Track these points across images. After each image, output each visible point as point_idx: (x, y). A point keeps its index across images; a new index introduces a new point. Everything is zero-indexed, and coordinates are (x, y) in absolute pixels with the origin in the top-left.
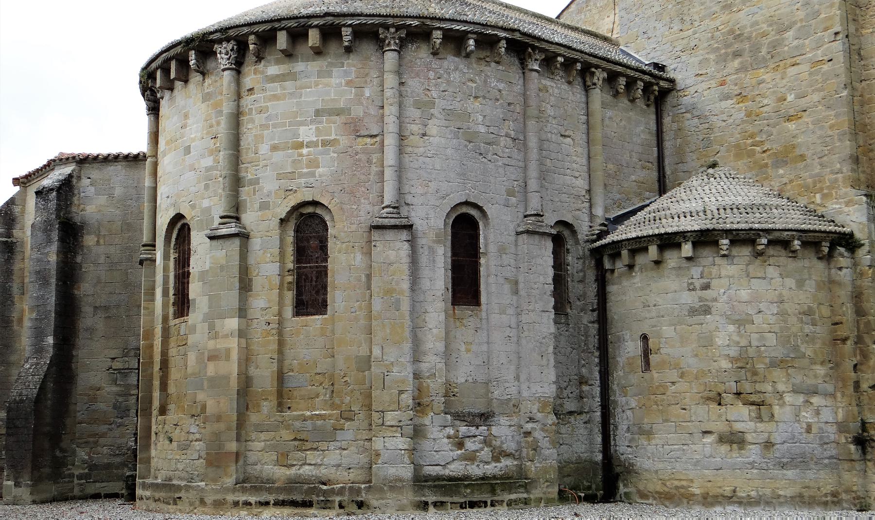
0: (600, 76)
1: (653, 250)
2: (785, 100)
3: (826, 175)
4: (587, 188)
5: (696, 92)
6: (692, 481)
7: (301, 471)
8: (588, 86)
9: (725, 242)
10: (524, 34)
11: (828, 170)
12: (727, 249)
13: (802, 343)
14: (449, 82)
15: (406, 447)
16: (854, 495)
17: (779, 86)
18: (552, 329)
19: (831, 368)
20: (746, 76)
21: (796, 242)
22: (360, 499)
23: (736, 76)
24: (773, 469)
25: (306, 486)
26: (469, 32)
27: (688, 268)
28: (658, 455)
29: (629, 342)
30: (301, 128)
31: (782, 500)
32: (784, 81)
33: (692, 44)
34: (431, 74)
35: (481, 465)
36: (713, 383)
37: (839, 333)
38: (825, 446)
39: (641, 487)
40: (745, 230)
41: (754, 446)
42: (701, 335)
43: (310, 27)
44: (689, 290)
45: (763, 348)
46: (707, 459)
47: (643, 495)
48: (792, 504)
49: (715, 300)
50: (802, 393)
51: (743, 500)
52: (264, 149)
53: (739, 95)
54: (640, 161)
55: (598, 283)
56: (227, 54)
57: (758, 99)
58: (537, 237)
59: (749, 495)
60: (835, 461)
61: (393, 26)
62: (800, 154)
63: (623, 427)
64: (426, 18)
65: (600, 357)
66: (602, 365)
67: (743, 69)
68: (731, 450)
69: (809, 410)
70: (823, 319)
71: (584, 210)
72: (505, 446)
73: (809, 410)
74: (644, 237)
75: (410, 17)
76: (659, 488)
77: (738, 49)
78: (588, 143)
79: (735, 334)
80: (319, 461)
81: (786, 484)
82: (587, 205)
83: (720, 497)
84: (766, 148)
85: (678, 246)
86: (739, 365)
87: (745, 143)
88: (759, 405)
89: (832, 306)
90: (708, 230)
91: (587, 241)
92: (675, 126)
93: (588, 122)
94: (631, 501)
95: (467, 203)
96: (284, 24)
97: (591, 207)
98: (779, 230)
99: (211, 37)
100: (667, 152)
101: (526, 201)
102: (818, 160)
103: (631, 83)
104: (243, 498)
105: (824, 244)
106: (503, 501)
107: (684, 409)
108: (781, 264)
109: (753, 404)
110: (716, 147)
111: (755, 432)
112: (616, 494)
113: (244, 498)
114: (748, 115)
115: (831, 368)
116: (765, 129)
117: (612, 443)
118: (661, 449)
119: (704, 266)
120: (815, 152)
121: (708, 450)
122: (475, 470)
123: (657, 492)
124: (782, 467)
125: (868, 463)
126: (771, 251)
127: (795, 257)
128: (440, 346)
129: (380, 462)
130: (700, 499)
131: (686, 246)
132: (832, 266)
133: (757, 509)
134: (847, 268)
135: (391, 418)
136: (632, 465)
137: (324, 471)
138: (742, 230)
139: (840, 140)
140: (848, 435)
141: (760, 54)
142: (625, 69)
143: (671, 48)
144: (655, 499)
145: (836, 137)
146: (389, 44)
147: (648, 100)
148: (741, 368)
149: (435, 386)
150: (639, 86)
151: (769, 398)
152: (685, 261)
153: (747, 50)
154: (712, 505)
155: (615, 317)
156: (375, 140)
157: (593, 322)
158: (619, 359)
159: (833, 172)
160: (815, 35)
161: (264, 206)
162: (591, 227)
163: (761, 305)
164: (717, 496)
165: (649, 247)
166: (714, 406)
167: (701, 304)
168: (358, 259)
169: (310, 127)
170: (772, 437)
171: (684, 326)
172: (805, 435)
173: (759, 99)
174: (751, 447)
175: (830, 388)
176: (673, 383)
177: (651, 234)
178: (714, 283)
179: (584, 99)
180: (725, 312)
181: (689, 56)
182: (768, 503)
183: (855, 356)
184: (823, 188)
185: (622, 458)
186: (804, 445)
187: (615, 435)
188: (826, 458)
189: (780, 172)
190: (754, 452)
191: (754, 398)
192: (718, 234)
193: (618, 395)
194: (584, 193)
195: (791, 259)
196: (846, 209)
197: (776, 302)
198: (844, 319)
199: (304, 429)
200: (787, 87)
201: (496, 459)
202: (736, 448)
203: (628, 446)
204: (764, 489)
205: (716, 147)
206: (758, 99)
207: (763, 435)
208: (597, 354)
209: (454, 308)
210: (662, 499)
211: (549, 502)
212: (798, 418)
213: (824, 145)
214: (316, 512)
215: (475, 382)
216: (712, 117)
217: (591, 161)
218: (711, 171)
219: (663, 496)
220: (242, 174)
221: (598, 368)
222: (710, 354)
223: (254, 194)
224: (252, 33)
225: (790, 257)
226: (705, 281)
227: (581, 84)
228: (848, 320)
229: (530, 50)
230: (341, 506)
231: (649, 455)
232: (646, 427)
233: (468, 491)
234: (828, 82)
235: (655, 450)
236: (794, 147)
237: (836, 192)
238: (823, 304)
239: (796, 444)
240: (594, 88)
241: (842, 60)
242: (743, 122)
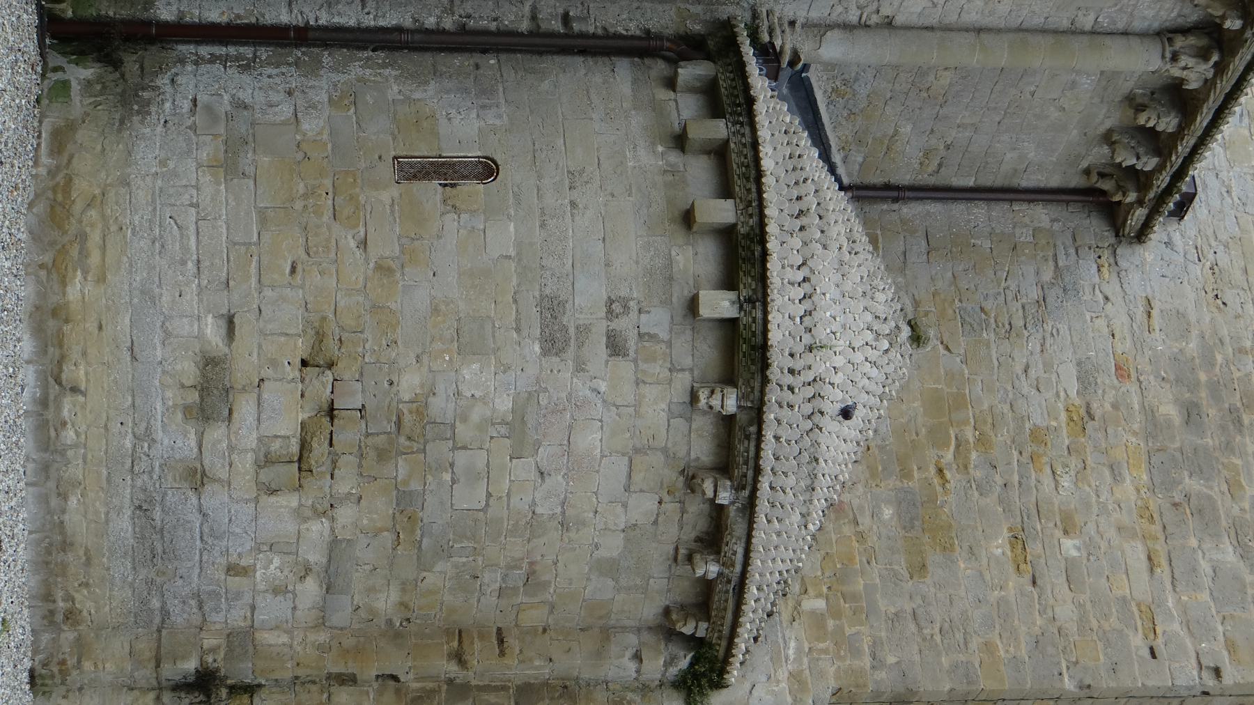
1: (723, 212)
2: (1066, 532)
3: (872, 627)
4: (900, 20)
5: (1107, 298)
6: (101, 279)
8: (1170, 40)
9: (731, 405)
11: (883, 634)
12: (711, 407)
13: (456, 566)
16: (71, 662)
17: (1102, 520)
19: (390, 622)
20: (1135, 434)
21: (713, 569)
23: (1136, 407)
24: (133, 487)
27: (666, 302)
28: (171, 191)
29: (477, 124)
32: (1112, 533)
33: (1229, 295)
36: (360, 349)
37: (477, 645)
38: (193, 602)
39: (82, 135)
40: (757, 456)
41: (193, 444)
42: (488, 327)
44: (610, 302)
45: (447, 477)
46: (159, 324)
47: (61, 140)
48: (44, 525)
49: (580, 368)
50: (329, 561)
51: (52, 409)
53: (1088, 413)
54: (948, 147)
55: (639, 38)
57: (1074, 462)
59: (64, 424)
60: (157, 620)
62: (928, 563)
63: (245, 86)
66: (417, 37)
67: (1153, 426)
68: (183, 386)
69: (286, 573)
70: (514, 612)
71: (839, 9)
73: (286, 573)
74: (760, 192)
76: (82, 187)
77: (1204, 416)
78: (1020, 30)
79: (489, 413)
81: (97, 512)
82: (853, 17)
83: (57, 352)
84: (948, 475)
85: (729, 282)
86: (407, 419)
87: (966, 422)
88: (300, 460)
89: (545, 630)
90: (765, 365)
91: (755, 15)
92: (1024, 236)
93: (1074, 32)
94: (45, 102)
97: (847, 27)
98: (749, 537)
100: (958, 210)
102: (908, 607)
103: (1158, 143)
105: (703, 625)
107: (293, 270)
108: (661, 528)
109: (304, 445)
110: (962, 344)
111: (231, 448)
112: (64, 54)
114: (1038, 436)
115: (390, 622)
116: (998, 478)
117: (204, 51)
118: (185, 199)
119: (669, 344)
120: (929, 604)
121: (184, 327)
123: (69, 180)
124: (140, 507)
125: (152, 695)
126: (696, 508)
127: (675, 560)
130: (54, 299)
131: (727, 304)
132: (647, 637)
133: (27, 443)
134: (638, 671)
136: (144, 112)
138: (758, 449)
139: (955, 667)
140: (222, 655)
141: (1186, 473)
142: (1199, 133)
143: (1223, 237)
144: (52, 173)
145: (962, 658)
147: (1102, 175)
148: (399, 423)
150: (1144, 159)
151: (318, 487)
152: (686, 293)
153: (1199, 442)
154: (38, 330)
155: (546, 85)
157: (534, 18)
158: (432, 86)
159: (876, 644)
160: (1218, 619)
162: (792, 23)
163: (560, 478)
164: (61, 346)
165: (730, 202)
166: (301, 348)
167: (572, 331)
170: (216, 486)
171: (514, 282)
172: (222, 561)
173: (1073, 466)
174: (192, 436)
175: (341, 616)
176: (364, 244)
177: (767, 212)
178: (625, 368)
179: (1138, 25)
180: (546, 390)
181: (1200, 286)
182: (45, 469)
183: (418, 679)
184: (840, 619)
185: (163, 81)
186: (197, 558)
187: (224, 60)
188: (164, 603)
189: (887, 512)
190: (179, 443)
191: (319, 448)
192: (753, 388)
193: (335, 77)
194: (886, 11)
195: (672, 552)
196: (783, 674)
197: (563, 513)
198: (511, 661)
200: (1098, 539)
202: (189, 400)
203: (195, 101)
204: (80, 461)
205: (962, 344)
206: (1074, 462)
207: (223, 466)
208: (448, 24)
210: (50, 194)
212: (265, 548)
213: (946, 625)
216: (1039, 336)
217: (971, 37)
218: (906, 332)
219: (60, 197)
221: (408, 23)
222: (438, 345)
225: (677, 549)
226: (632, 344)
227: (1180, 20)
228: (509, 668)
231: (171, 165)
232: (247, 160)
234: (1100, 646)
235: (184, 182)
236: (947, 549)
237: (825, 651)
238: (551, 612)
239: (198, 542)
240: (1163, 57)
241: (1150, 683)
242: (1021, 420)
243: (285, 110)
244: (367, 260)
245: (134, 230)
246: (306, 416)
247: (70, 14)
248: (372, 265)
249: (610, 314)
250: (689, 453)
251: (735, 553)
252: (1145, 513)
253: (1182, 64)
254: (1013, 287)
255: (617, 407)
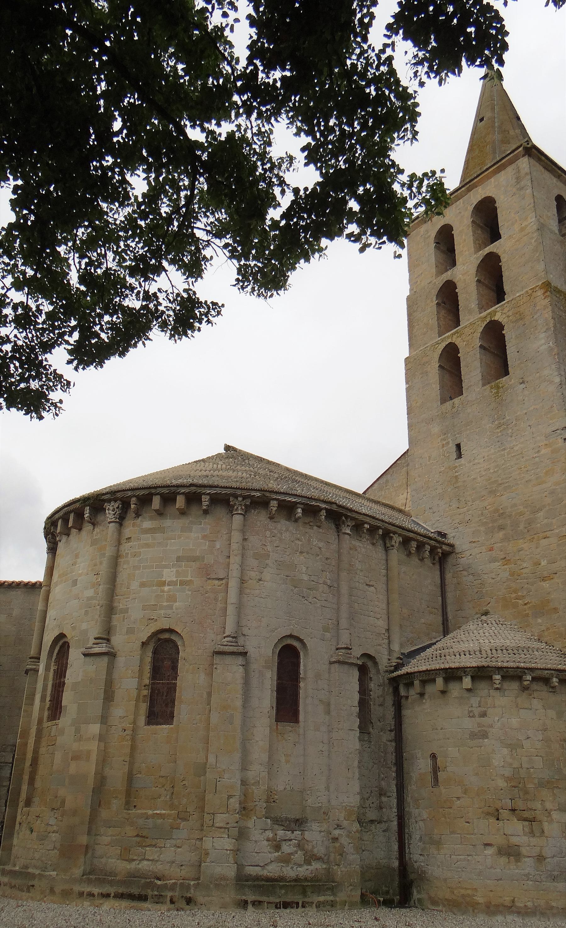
0: (397, 540)
1: (440, 681)
2: (540, 564)
6: (476, 889)
7: (140, 866)
9: (498, 677)
10: (340, 506)
14: (280, 539)
15: (231, 847)
18: (357, 745)
20: (509, 545)
22: (189, 895)
25: (143, 881)
26: (298, 503)
30: (165, 570)
31: (555, 911)
34: (268, 533)
35: (295, 868)
40: (513, 668)
43: (179, 493)
45: (532, 770)
47: (435, 902)
49: (491, 726)
52: (135, 585)
54: (428, 607)
56: (113, 510)
57: (519, 562)
58: (346, 667)
59: (525, 905)
61: (241, 495)
63: (416, 836)
64: (266, 491)
65: (397, 772)
66: (399, 779)
68: (509, 862)
71: (384, 646)
72: (315, 851)
74: (432, 670)
75: (254, 490)
80: (156, 857)
82: (386, 641)
85: (460, 679)
86: (513, 784)
88: (531, 822)
91: (387, 671)
93: (387, 575)
95: (291, 636)
96: (159, 490)
97: (389, 643)
98: (540, 669)
99: (103, 497)
101: (338, 637)
103: (420, 546)
104: (87, 889)
106: (312, 903)
109: (525, 820)
111: (529, 846)
112: (411, 900)
113: (88, 890)
114: (512, 574)
119: (481, 697)
122: (290, 872)
126: (535, 686)
128: (265, 757)
129: (208, 860)
135: (220, 819)
136: (424, 872)
137: (160, 867)
138: (510, 668)
141: (519, 529)
144: (444, 906)
146: (237, 509)
147: (434, 559)
148: (515, 787)
149: (259, 792)
150: (426, 549)
156: (221, 582)
157: (391, 741)
161: (130, 631)
162: (389, 660)
166: (492, 820)
167: (480, 729)
168: (202, 678)
169: (172, 569)
171: (466, 748)
176: (458, 798)
178: (490, 711)
179: (384, 557)
182: (543, 914)
185: (416, 865)
187: (409, 844)
191: (526, 814)
193: (411, 807)
199: (146, 826)
201: (308, 862)
203: (421, 855)
206: (519, 562)
208: (394, 769)
209: (277, 724)
211: (352, 905)
214: (150, 906)
215: (292, 790)
216: (483, 575)
218: (484, 618)
220: (116, 604)
221: (395, 782)
223: (124, 621)
224: (134, 496)
225: (550, 692)
229: (344, 518)
230: (172, 902)
231: (439, 863)
233: (283, 891)
243: (421, 824)
244: (463, 797)
245: (460, 878)
246: (516, 819)
247: (398, 897)
248: (464, 795)
249: (473, 716)
250: (516, 689)
251: (547, 673)
252: (531, 540)
253: (394, 544)
254: (470, 583)
255: (503, 713)
